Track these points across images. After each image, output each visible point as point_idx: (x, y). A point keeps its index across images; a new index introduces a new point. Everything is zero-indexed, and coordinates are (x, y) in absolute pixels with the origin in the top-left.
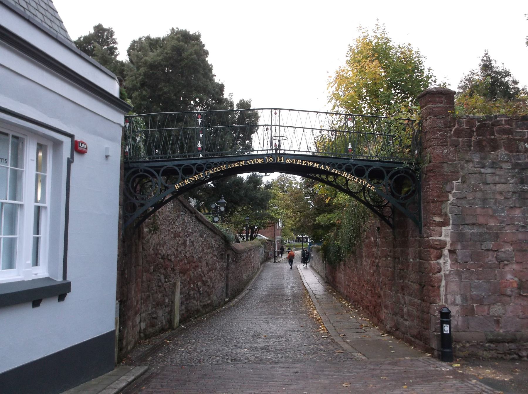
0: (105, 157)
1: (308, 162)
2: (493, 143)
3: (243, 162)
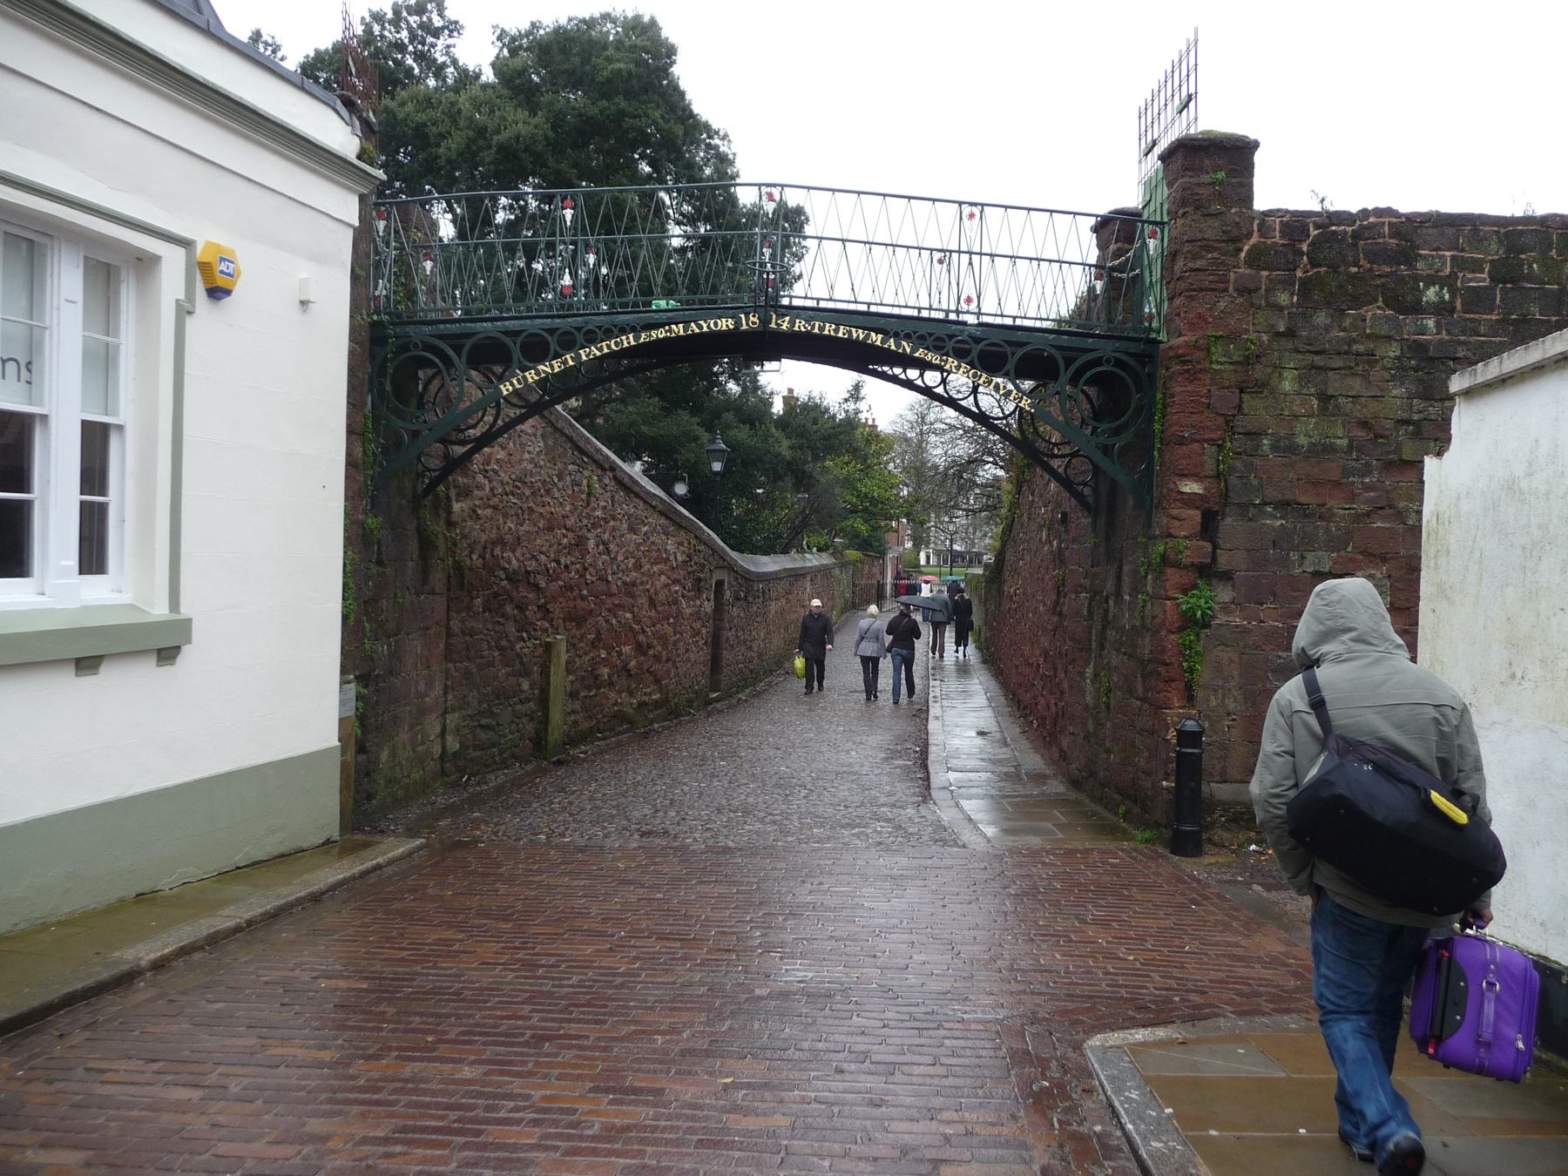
0: (298, 303)
1: (854, 330)
2: (1353, 286)
3: (681, 326)
